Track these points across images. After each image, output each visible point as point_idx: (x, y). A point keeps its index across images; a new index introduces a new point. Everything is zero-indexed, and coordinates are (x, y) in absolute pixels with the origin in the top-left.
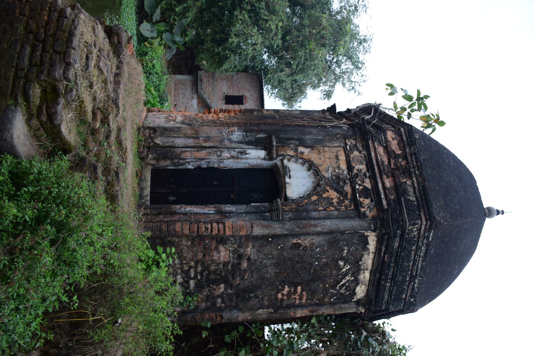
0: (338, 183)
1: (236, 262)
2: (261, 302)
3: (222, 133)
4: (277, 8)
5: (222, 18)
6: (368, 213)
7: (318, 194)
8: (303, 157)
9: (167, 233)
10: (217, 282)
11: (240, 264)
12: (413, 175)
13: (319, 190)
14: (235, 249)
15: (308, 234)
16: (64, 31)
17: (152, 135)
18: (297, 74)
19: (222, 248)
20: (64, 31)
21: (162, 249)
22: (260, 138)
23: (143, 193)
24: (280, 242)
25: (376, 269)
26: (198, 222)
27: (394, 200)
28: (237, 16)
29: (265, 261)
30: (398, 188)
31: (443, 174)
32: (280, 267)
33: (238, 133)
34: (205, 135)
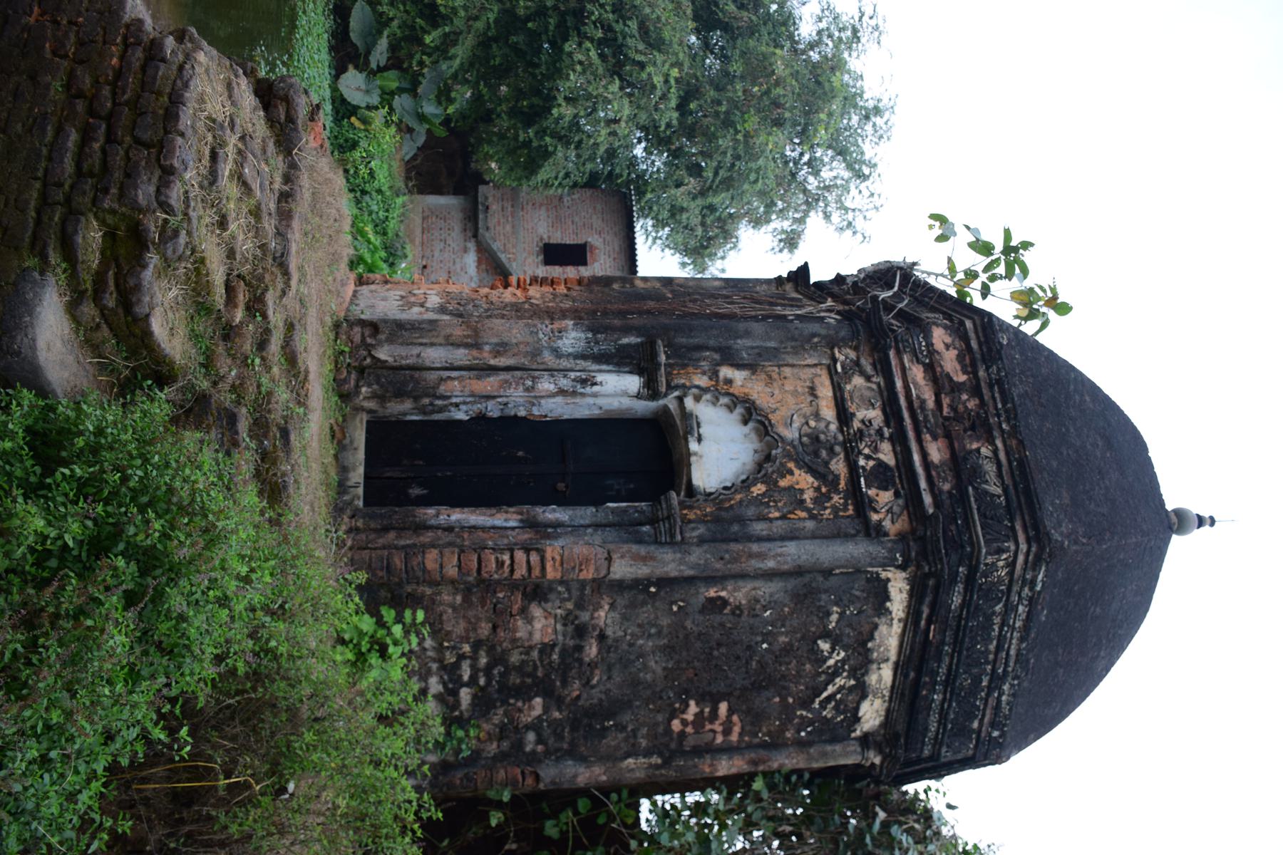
0: (816, 454)
1: (571, 643)
2: (632, 741)
3: (537, 333)
4: (666, 34)
5: (536, 60)
6: (887, 524)
7: (767, 480)
8: (731, 391)
9: (404, 575)
10: (524, 693)
11: (579, 648)
12: (996, 433)
13: (770, 470)
14: (569, 613)
15: (743, 576)
16: (159, 94)
17: (369, 340)
18: (716, 192)
19: (536, 611)
20: (159, 94)
21: (393, 613)
22: (629, 345)
23: (347, 479)
24: (677, 596)
25: (909, 660)
26: (480, 549)
27: (949, 492)
28: (570, 54)
29: (641, 642)
30: (961, 465)
31: (1068, 430)
32: (676, 657)
33: (574, 334)
34: (495, 340)
